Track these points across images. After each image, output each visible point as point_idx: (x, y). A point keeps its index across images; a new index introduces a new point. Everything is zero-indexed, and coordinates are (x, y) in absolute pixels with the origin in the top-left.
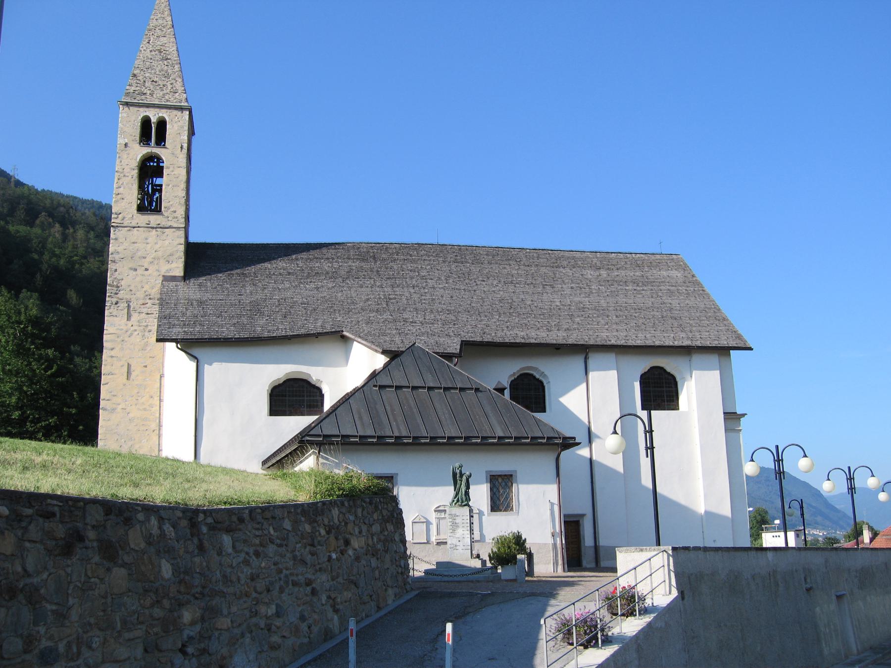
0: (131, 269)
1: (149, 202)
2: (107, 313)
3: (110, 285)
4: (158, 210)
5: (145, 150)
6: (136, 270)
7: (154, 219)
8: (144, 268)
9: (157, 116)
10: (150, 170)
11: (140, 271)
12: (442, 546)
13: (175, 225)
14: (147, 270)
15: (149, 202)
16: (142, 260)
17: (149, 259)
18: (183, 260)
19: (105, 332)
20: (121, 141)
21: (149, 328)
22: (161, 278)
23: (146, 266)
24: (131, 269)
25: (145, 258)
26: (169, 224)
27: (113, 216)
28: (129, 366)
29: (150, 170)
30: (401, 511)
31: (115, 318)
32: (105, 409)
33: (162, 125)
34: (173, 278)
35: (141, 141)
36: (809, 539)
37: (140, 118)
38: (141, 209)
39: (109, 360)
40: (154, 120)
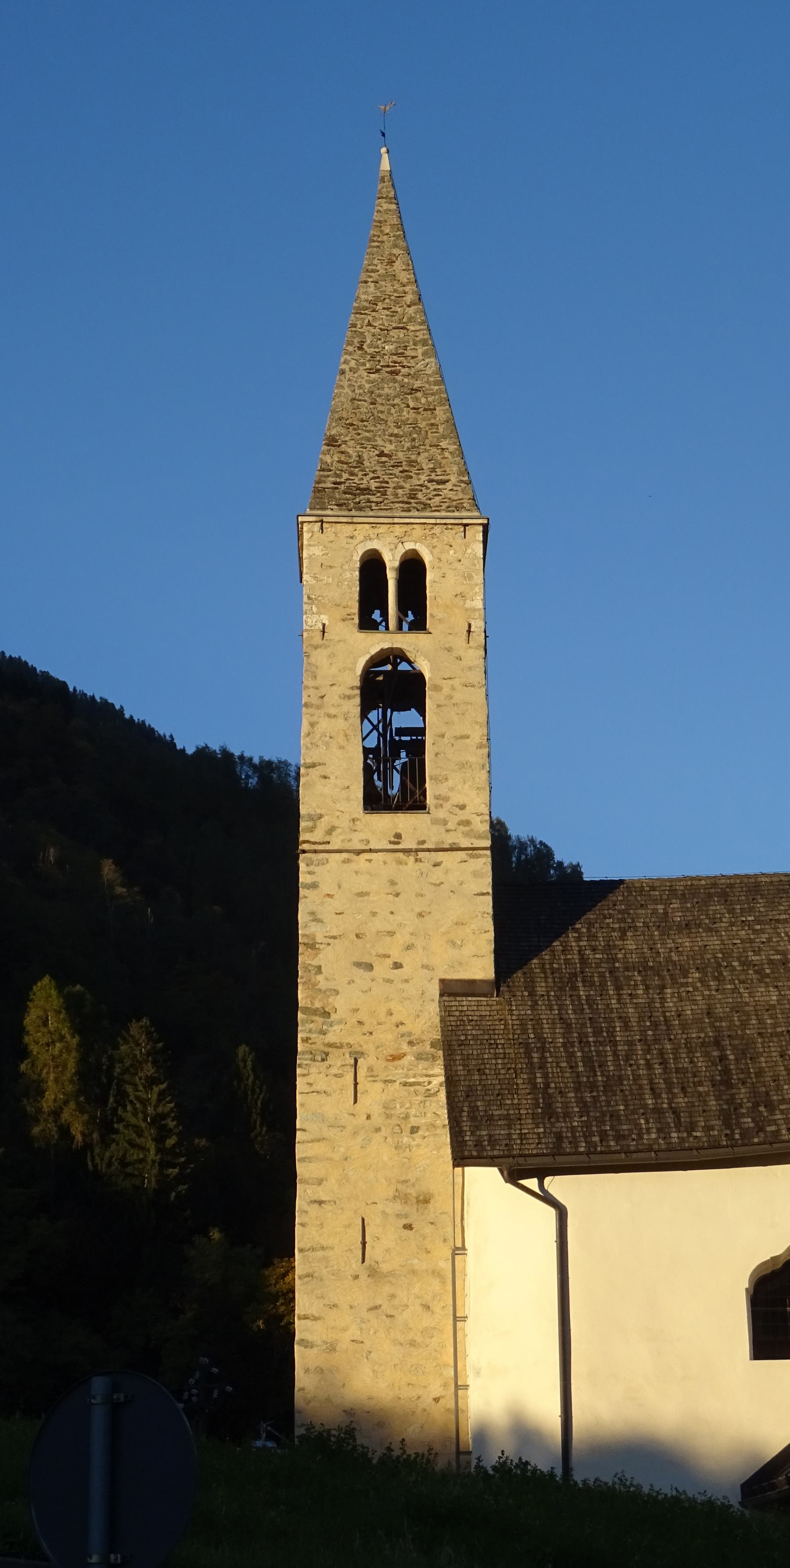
0: (358, 965)
1: (395, 777)
2: (300, 1083)
3: (306, 1010)
4: (413, 800)
5: (376, 643)
6: (369, 967)
7: (405, 823)
8: (389, 962)
9: (401, 551)
10: (391, 687)
11: (382, 969)
12: (364, 960)
13: (465, 843)
14: (397, 966)
15: (395, 777)
16: (386, 932)
17: (402, 938)
18: (491, 935)
19: (299, 1136)
20: (312, 620)
21: (413, 1121)
22: (435, 990)
23: (396, 956)
24: (358, 965)
25: (391, 934)
26: (449, 840)
27: (303, 824)
28: (363, 1220)
29: (391, 687)
30: (46, 675)
31: (322, 1098)
32: (305, 1343)
33: (413, 569)
34: (469, 988)
35: (365, 809)
36: (321, 947)
37: (357, 558)
38: (375, 801)
39: (314, 1210)
40: (392, 561)
